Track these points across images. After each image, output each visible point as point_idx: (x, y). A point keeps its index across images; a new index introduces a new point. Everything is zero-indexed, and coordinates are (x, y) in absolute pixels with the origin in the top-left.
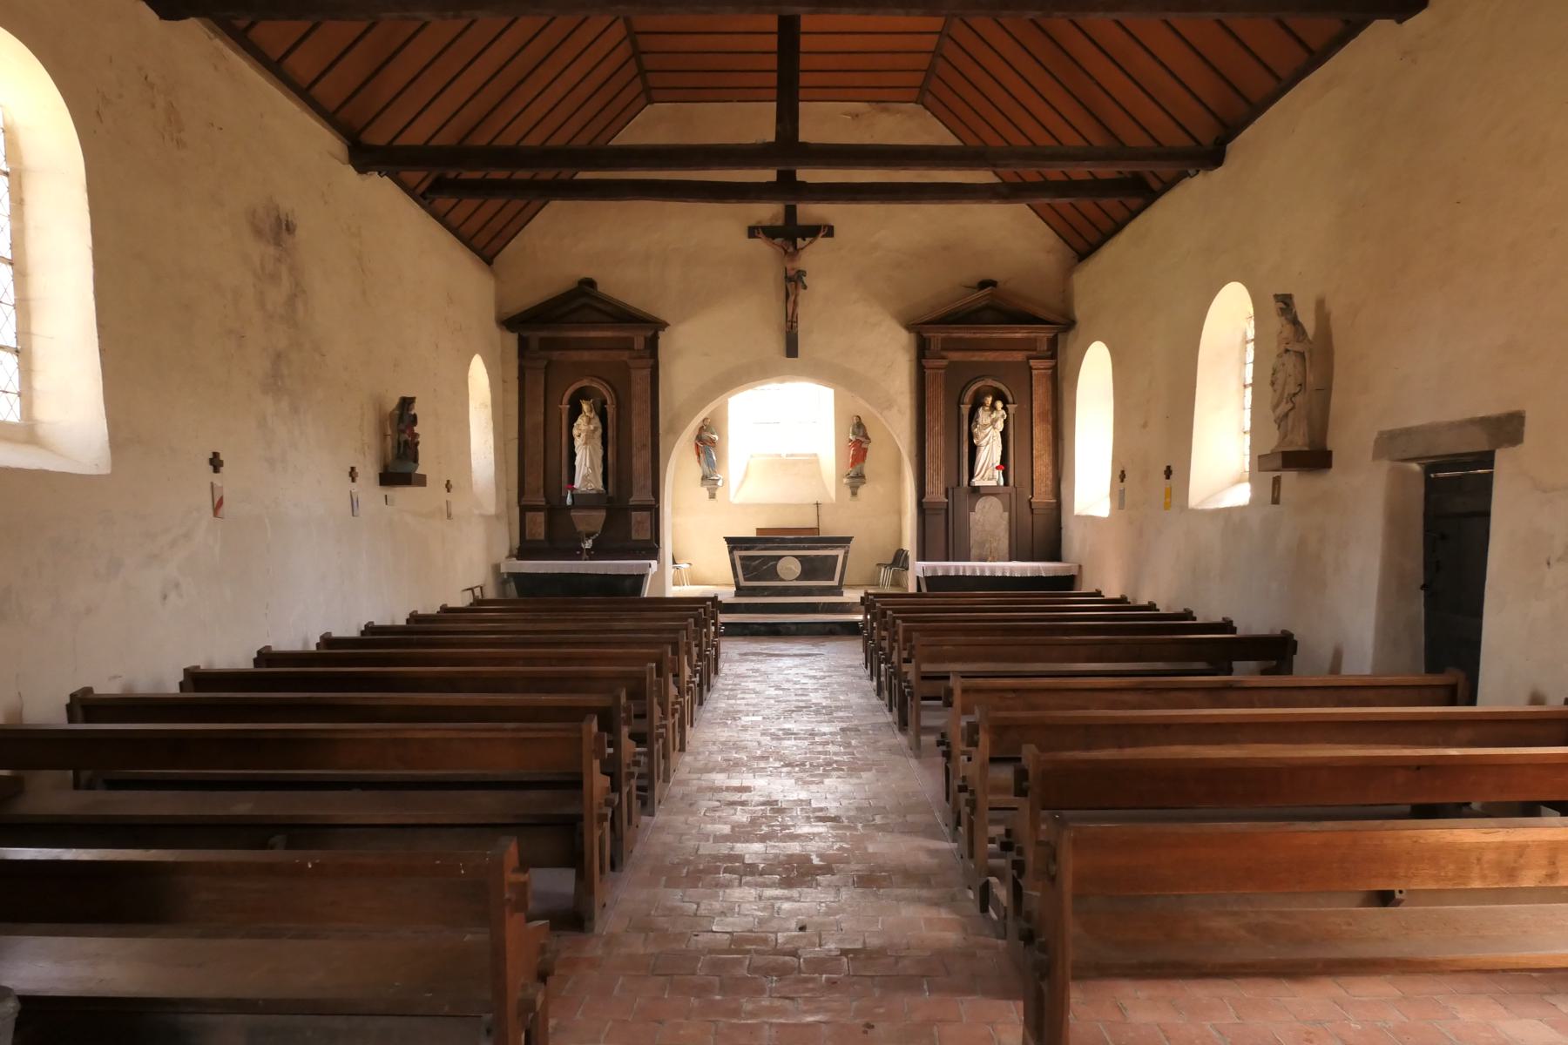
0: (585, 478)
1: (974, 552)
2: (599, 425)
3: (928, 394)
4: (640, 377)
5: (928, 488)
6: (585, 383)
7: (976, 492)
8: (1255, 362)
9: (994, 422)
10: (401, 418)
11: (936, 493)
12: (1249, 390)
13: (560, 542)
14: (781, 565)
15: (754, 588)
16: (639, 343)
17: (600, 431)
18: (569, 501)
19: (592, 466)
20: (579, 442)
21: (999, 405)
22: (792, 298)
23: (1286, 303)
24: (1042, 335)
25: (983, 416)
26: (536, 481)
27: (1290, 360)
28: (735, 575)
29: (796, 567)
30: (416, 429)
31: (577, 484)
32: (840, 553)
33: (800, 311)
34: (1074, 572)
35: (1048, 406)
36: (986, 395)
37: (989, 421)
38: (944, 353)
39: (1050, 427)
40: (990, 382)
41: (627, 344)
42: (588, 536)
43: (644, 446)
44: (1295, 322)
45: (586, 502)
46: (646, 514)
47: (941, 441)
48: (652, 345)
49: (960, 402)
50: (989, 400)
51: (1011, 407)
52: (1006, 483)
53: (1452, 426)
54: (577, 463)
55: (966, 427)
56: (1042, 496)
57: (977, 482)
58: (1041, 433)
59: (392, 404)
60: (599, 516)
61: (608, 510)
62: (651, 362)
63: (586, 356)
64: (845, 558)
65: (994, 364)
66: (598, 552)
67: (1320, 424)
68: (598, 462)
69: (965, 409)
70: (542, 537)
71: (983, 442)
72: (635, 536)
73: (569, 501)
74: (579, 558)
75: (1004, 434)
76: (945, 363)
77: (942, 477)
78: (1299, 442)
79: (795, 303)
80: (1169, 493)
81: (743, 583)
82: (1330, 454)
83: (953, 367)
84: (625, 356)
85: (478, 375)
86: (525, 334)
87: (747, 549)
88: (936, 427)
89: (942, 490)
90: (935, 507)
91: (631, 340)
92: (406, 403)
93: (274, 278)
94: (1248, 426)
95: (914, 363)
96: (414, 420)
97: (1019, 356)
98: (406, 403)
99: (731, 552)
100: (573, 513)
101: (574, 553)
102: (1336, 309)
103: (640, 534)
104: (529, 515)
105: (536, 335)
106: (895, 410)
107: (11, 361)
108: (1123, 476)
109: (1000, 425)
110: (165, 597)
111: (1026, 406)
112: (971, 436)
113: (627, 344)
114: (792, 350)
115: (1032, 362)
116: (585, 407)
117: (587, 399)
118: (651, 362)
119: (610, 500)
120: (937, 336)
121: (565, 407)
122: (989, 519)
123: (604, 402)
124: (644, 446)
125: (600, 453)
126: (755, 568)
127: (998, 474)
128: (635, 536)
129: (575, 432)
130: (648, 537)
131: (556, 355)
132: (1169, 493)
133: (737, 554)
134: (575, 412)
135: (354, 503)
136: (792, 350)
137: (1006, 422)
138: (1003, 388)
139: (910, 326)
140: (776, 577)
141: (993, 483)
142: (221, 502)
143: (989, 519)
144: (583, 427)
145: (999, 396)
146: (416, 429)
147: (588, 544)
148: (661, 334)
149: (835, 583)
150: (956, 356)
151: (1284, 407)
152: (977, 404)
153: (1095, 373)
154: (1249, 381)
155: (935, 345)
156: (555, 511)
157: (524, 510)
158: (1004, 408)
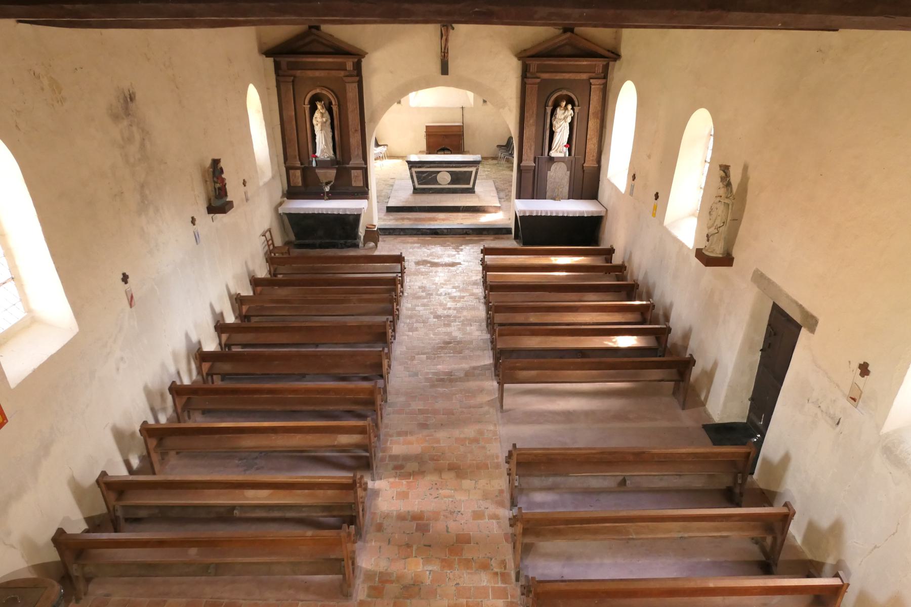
0: (322, 151)
1: (548, 194)
2: (329, 117)
3: (528, 100)
4: (351, 90)
5: (524, 157)
6: (318, 91)
7: (552, 160)
8: (713, 150)
9: (565, 118)
10: (214, 172)
11: (529, 162)
12: (708, 165)
13: (310, 190)
14: (439, 177)
15: (424, 189)
16: (350, 65)
17: (329, 121)
18: (314, 164)
19: (326, 144)
20: (317, 129)
21: (570, 107)
22: (444, 38)
23: (725, 169)
24: (599, 63)
25: (560, 112)
26: (293, 151)
27: (721, 207)
28: (413, 182)
29: (448, 178)
30: (223, 176)
31: (318, 154)
32: (473, 169)
33: (450, 44)
34: (603, 214)
35: (599, 108)
36: (562, 101)
37: (563, 117)
38: (538, 75)
39: (599, 121)
40: (565, 92)
41: (342, 67)
42: (327, 184)
43: (356, 130)
44: (729, 185)
45: (322, 164)
46: (360, 172)
47: (533, 129)
48: (358, 67)
49: (546, 105)
50: (564, 104)
51: (576, 109)
52: (570, 154)
53: (788, 296)
54: (317, 141)
55: (548, 121)
56: (590, 163)
57: (553, 154)
58: (593, 124)
59: (208, 163)
60: (333, 172)
61: (337, 169)
62: (357, 79)
63: (317, 73)
64: (476, 173)
65: (569, 80)
66: (335, 194)
67: (730, 241)
68: (330, 140)
69: (549, 110)
70: (300, 184)
71: (558, 130)
72: (354, 184)
73: (314, 164)
74: (321, 198)
75: (571, 125)
76: (538, 80)
77: (533, 151)
78: (717, 251)
79: (447, 40)
80: (655, 208)
81: (417, 186)
82: (732, 259)
83: (544, 84)
84: (342, 73)
85: (253, 98)
86: (278, 59)
87: (420, 167)
88: (530, 122)
89: (532, 158)
90: (528, 169)
91: (345, 64)
92: (216, 162)
93: (130, 140)
94: (703, 186)
95: (520, 79)
96: (222, 171)
97: (584, 76)
98: (216, 162)
99: (410, 169)
100: (317, 171)
101: (318, 195)
102: (753, 175)
103: (357, 182)
104: (291, 172)
105: (285, 60)
106: (507, 108)
107: (11, 285)
108: (634, 177)
109: (569, 120)
110: (118, 369)
111: (586, 108)
112: (551, 125)
113: (342, 67)
114: (445, 70)
115: (591, 81)
116: (319, 107)
117: (320, 101)
118: (357, 79)
119: (338, 163)
120: (534, 64)
121: (307, 107)
122: (558, 175)
123: (331, 103)
124: (356, 130)
125: (330, 135)
126: (424, 178)
127: (566, 150)
128: (354, 184)
129: (314, 122)
130: (361, 184)
131: (298, 73)
132: (655, 208)
133: (414, 170)
134: (313, 109)
135: (197, 237)
136: (445, 70)
137: (573, 118)
138: (573, 96)
139: (519, 58)
140: (436, 182)
141: (562, 155)
142: (132, 297)
143: (558, 175)
144: (319, 120)
145: (570, 101)
146: (223, 176)
147: (327, 189)
148: (363, 60)
149: (470, 186)
150: (545, 76)
151: (713, 230)
152: (556, 105)
153: (626, 101)
154: (708, 160)
155: (533, 68)
156: (307, 171)
157: (288, 169)
158: (573, 109)
